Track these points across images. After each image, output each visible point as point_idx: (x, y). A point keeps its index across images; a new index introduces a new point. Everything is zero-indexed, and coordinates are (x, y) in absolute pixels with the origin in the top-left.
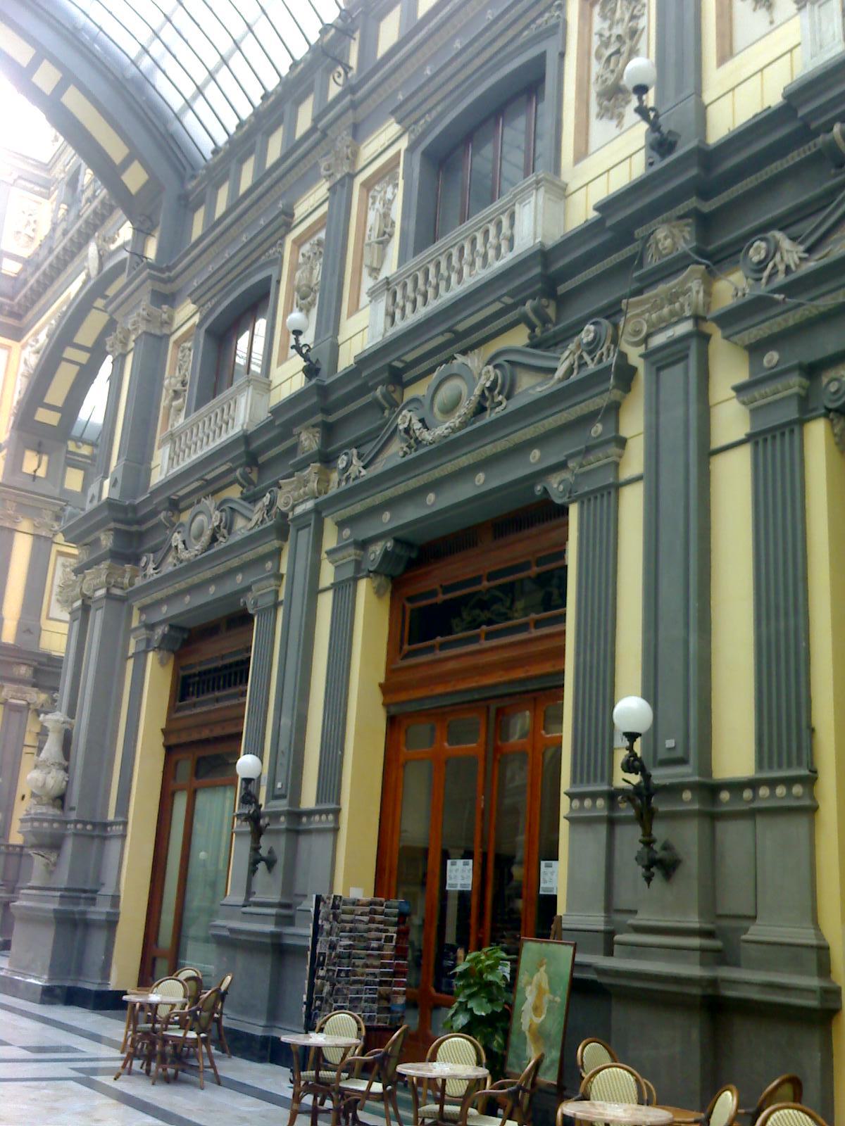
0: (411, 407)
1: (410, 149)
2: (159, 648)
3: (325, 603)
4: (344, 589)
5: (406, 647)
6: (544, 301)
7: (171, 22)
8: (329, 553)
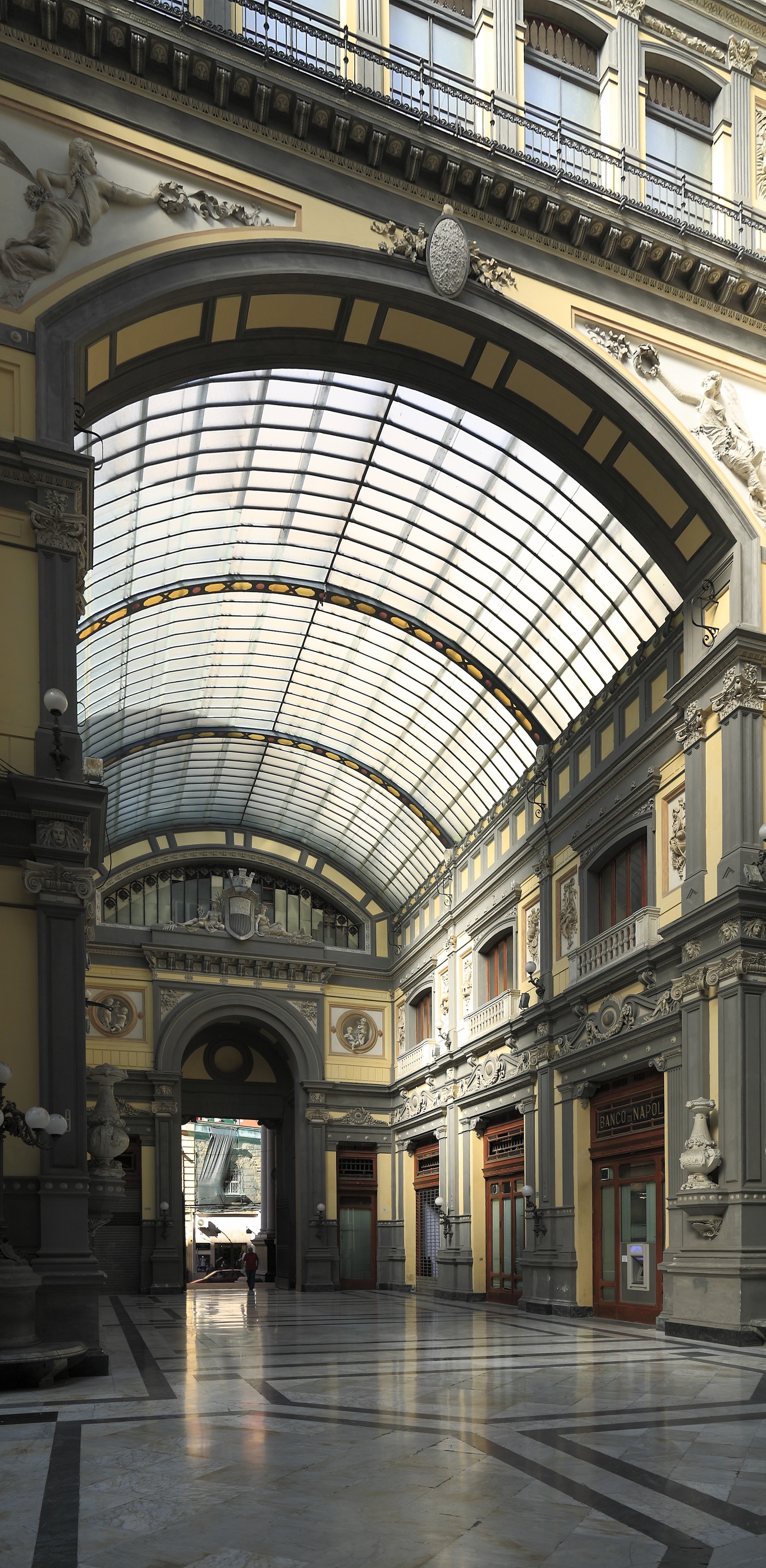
0: (591, 1018)
1: (582, 867)
2: (581, 1097)
3: (558, 1110)
4: (567, 1103)
5: (598, 1132)
6: (582, 1007)
7: (440, 681)
8: (558, 1087)
